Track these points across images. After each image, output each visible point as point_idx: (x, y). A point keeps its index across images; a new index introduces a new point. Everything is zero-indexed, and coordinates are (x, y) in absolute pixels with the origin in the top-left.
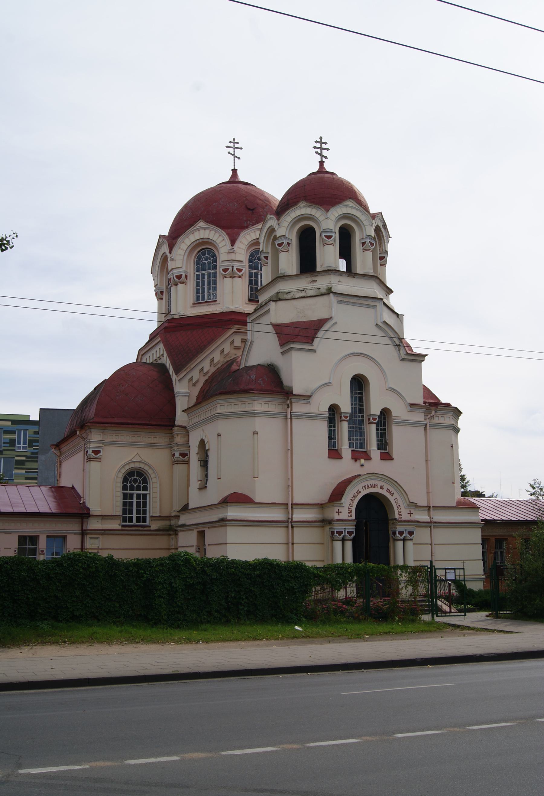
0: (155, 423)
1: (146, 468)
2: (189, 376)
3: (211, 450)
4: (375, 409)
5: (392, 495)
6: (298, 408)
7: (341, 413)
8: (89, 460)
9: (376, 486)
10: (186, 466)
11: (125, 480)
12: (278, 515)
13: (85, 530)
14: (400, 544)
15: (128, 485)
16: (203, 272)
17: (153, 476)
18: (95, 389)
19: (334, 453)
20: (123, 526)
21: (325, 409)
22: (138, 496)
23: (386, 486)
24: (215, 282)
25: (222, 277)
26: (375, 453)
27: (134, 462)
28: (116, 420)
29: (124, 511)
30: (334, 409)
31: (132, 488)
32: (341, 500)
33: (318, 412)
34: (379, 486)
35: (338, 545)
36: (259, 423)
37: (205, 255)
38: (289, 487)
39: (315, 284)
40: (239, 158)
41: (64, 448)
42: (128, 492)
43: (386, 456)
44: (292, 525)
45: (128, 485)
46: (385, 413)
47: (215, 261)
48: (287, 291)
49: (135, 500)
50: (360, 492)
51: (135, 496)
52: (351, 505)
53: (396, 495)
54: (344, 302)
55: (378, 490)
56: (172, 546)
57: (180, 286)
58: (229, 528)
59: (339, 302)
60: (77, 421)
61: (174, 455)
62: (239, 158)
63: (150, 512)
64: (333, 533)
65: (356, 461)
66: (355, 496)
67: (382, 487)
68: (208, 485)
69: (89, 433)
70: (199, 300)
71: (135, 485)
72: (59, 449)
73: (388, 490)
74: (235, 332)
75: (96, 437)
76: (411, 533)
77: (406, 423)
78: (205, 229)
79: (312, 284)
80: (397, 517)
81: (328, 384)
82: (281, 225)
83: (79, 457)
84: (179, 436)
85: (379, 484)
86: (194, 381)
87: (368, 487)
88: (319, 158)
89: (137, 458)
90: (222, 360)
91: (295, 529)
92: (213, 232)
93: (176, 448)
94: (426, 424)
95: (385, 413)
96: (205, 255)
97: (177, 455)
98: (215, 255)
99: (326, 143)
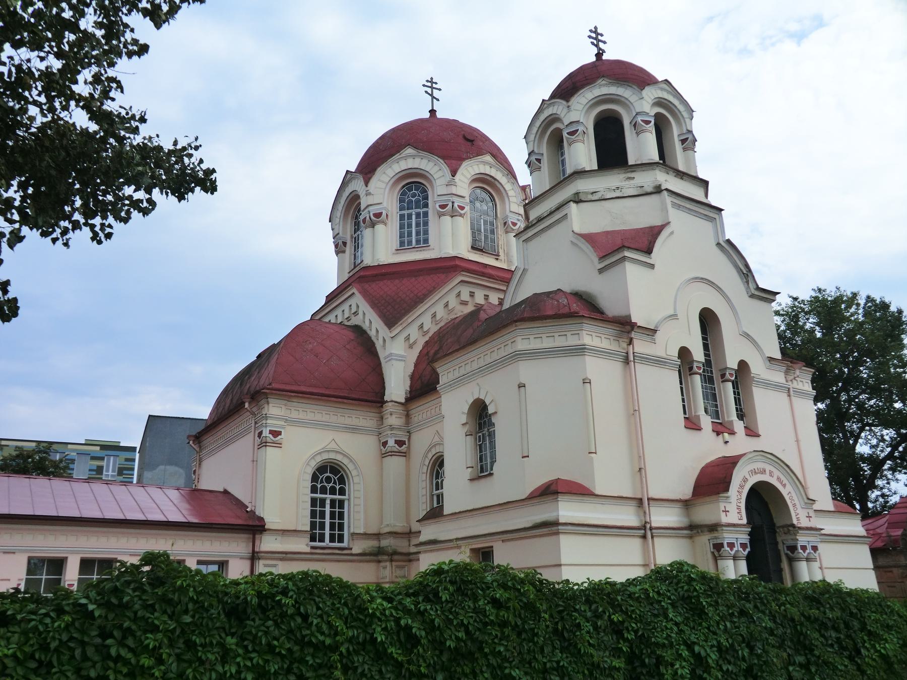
0: (357, 397)
1: (345, 461)
2: (405, 334)
3: (499, 414)
4: (732, 363)
6: (641, 346)
7: (693, 361)
8: (264, 444)
10: (402, 460)
11: (315, 478)
12: (627, 517)
13: (257, 553)
15: (319, 486)
16: (410, 211)
17: (354, 473)
18: (259, 357)
20: (312, 548)
22: (333, 502)
23: (777, 473)
24: (426, 224)
25: (437, 217)
26: (739, 426)
27: (328, 451)
28: (303, 389)
29: (313, 525)
31: (323, 491)
32: (728, 490)
33: (665, 356)
34: (767, 472)
36: (593, 366)
37: (414, 189)
39: (632, 182)
40: (438, 100)
41: (208, 440)
42: (319, 495)
43: (752, 432)
45: (319, 486)
46: (743, 365)
47: (426, 198)
48: (592, 191)
49: (328, 509)
51: (328, 502)
56: (383, 578)
57: (379, 228)
58: (562, 537)
60: (232, 400)
61: (385, 444)
62: (438, 100)
63: (349, 527)
64: (718, 547)
65: (718, 434)
68: (495, 470)
69: (266, 406)
70: (404, 244)
71: (328, 486)
72: (199, 443)
74: (462, 281)
75: (276, 411)
77: (767, 385)
78: (413, 157)
79: (627, 183)
80: (795, 522)
82: (572, 108)
83: (248, 442)
84: (394, 416)
85: (768, 468)
86: (411, 341)
88: (595, 51)
89: (333, 446)
90: (446, 317)
91: (655, 539)
92: (425, 161)
93: (389, 432)
96: (414, 189)
97: (391, 443)
98: (425, 191)
99: (602, 35)
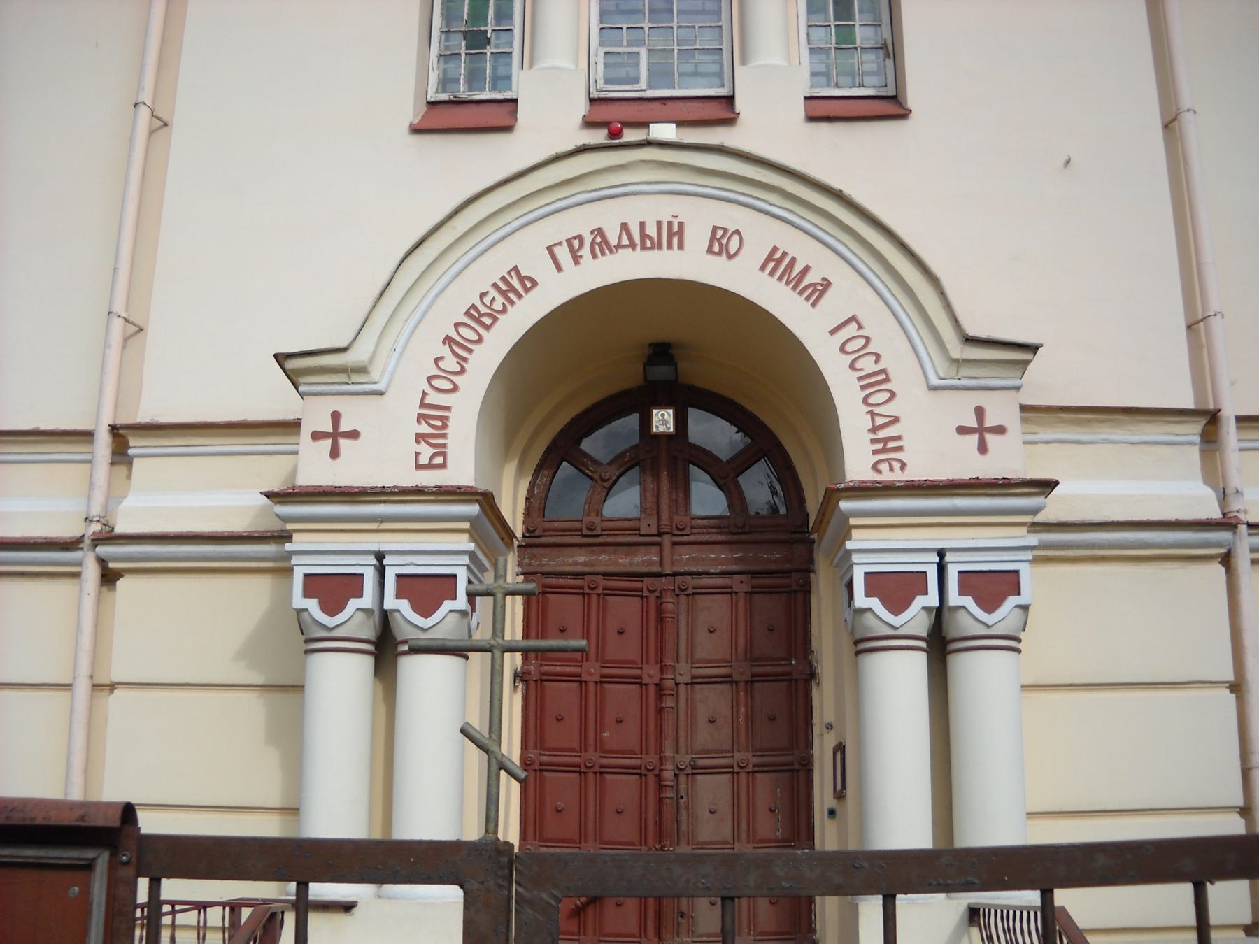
5: (818, 292)
9: (674, 235)
14: (898, 680)
23: (761, 234)
34: (697, 237)
35: (341, 679)
44: (102, 562)
50: (530, 283)
52: (445, 379)
53: (850, 294)
55: (689, 264)
66: (481, 317)
73: (776, 263)
76: (993, 587)
85: (700, 218)
87: (601, 244)
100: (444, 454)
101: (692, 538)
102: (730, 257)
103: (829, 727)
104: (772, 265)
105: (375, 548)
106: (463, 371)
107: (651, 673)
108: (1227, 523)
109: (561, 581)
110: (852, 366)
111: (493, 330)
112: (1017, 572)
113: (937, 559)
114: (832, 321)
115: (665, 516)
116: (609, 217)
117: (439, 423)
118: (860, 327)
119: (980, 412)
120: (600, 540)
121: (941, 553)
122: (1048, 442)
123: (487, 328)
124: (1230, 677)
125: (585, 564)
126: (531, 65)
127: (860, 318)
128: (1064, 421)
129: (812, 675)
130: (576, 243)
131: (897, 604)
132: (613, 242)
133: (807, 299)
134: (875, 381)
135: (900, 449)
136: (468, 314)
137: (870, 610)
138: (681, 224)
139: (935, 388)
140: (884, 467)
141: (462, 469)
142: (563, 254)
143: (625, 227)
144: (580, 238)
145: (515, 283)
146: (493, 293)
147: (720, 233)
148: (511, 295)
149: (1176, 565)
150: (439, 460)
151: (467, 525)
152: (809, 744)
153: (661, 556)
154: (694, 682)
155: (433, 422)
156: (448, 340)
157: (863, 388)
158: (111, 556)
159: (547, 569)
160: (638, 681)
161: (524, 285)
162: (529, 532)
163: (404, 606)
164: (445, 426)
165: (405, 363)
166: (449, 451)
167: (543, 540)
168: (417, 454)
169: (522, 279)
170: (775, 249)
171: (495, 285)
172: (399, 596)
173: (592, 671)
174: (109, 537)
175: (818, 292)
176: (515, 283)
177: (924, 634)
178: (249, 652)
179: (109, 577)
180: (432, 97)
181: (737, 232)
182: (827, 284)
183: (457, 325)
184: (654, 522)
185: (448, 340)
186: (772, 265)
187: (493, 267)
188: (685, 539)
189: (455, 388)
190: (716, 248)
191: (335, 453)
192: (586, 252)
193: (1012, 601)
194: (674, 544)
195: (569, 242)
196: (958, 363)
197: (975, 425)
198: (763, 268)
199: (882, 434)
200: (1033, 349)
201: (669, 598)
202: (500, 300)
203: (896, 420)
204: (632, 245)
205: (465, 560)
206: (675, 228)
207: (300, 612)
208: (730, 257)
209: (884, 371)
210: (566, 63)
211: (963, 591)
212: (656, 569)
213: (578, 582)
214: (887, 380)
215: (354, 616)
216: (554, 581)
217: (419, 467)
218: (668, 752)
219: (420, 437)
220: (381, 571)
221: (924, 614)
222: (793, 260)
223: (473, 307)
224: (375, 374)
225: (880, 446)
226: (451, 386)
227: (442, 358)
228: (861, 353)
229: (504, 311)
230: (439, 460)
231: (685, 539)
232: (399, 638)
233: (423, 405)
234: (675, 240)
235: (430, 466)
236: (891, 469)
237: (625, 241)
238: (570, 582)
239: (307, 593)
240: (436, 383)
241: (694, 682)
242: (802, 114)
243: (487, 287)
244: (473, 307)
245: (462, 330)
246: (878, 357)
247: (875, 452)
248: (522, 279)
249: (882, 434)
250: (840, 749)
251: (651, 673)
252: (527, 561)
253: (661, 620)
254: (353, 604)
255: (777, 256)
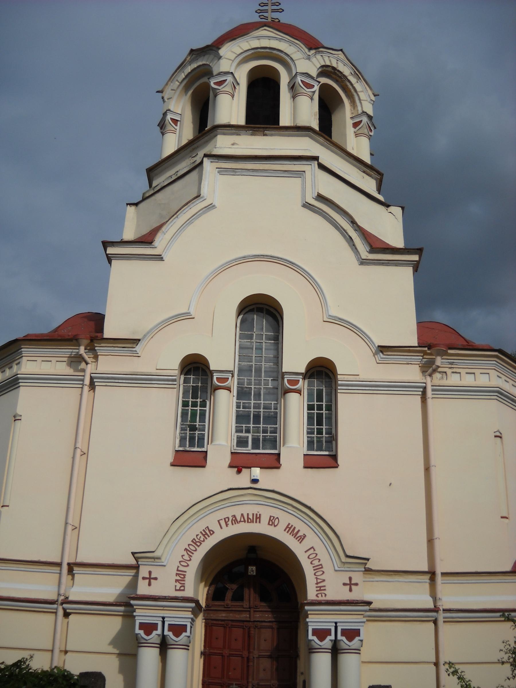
5: (302, 539)
6: (108, 363)
9: (258, 518)
19: (190, 455)
21: (172, 364)
23: (285, 519)
30: (195, 367)
34: (265, 519)
38: (70, 527)
44: (64, 610)
50: (212, 532)
52: (185, 562)
53: (312, 539)
54: (234, 172)
55: (261, 528)
59: (222, 171)
66: (196, 543)
67: (272, 521)
73: (290, 529)
76: (352, 634)
81: (186, 316)
85: (266, 513)
87: (235, 521)
94: (425, 388)
95: (322, 371)
100: (184, 586)
101: (260, 609)
102: (275, 526)
103: (302, 673)
104: (288, 529)
105: (162, 615)
106: (190, 560)
107: (245, 654)
108: (436, 610)
109: (217, 622)
110: (311, 563)
111: (200, 547)
112: (359, 629)
113: (334, 625)
114: (306, 549)
115: (252, 602)
116: (237, 511)
117: (183, 576)
118: (314, 550)
119: (350, 579)
120: (230, 609)
121: (336, 623)
122: (377, 581)
123: (198, 546)
124: (434, 661)
125: (225, 617)
126: (212, 442)
127: (315, 547)
128: (383, 574)
129: (297, 656)
130: (227, 520)
131: (322, 639)
132: (239, 520)
133: (298, 541)
134: (318, 568)
135: (325, 590)
136: (192, 541)
137: (313, 640)
138: (260, 515)
139: (336, 571)
140: (320, 595)
141: (189, 593)
142: (223, 523)
143: (242, 515)
144: (228, 518)
145: (207, 532)
146: (200, 535)
147: (272, 518)
148: (206, 536)
149: (418, 623)
150: (182, 588)
151: (191, 609)
152: (296, 678)
153: (250, 615)
154: (260, 657)
155: (181, 576)
156: (186, 550)
157: (314, 570)
158: (66, 607)
159: (213, 618)
160: (241, 656)
161: (210, 533)
162: (207, 605)
163: (170, 634)
164: (184, 577)
165: (172, 555)
166: (186, 585)
167: (212, 608)
168: (176, 586)
169: (210, 531)
170: (289, 524)
171: (201, 532)
172: (169, 630)
173: (227, 652)
174: (66, 601)
175: (302, 539)
176: (207, 532)
177: (330, 647)
178: (114, 642)
179: (66, 615)
180: (177, 448)
181: (278, 518)
182: (305, 536)
183: (189, 545)
184: (248, 604)
185: (186, 550)
186: (288, 529)
187: (200, 527)
188: (258, 610)
189: (188, 565)
190: (271, 523)
191: (150, 584)
192: (230, 523)
193: (357, 638)
194: (254, 611)
195: (225, 519)
196: (344, 563)
197: (349, 583)
198: (285, 530)
199: (319, 585)
200: (368, 559)
201: (252, 629)
202: (202, 537)
203: (324, 580)
204: (245, 521)
205: (190, 620)
206: (258, 516)
207: (137, 634)
208: (275, 526)
209: (321, 565)
210: (223, 443)
211: (342, 635)
212: (248, 619)
213: (223, 623)
214: (322, 567)
215: (155, 636)
216: (215, 622)
217: (176, 590)
218: (250, 680)
219: (177, 581)
220: (163, 622)
221: (330, 642)
222: (295, 528)
223: (194, 539)
224: (163, 559)
225: (319, 589)
226: (186, 565)
227: (184, 555)
228: (314, 559)
229: (204, 541)
230: (182, 588)
231: (258, 610)
232: (168, 643)
233: (178, 570)
234: (258, 520)
235: (180, 590)
236: (322, 596)
237: (242, 520)
238: (220, 622)
239: (140, 629)
240: (182, 563)
241: (260, 657)
242: (302, 465)
243: (199, 533)
244: (194, 539)
245: (191, 547)
246: (319, 560)
247: (317, 591)
248: (210, 531)
249: (319, 585)
250: (304, 682)
251: (245, 654)
252: (206, 615)
253: (249, 637)
254: (155, 633)
255: (290, 526)
